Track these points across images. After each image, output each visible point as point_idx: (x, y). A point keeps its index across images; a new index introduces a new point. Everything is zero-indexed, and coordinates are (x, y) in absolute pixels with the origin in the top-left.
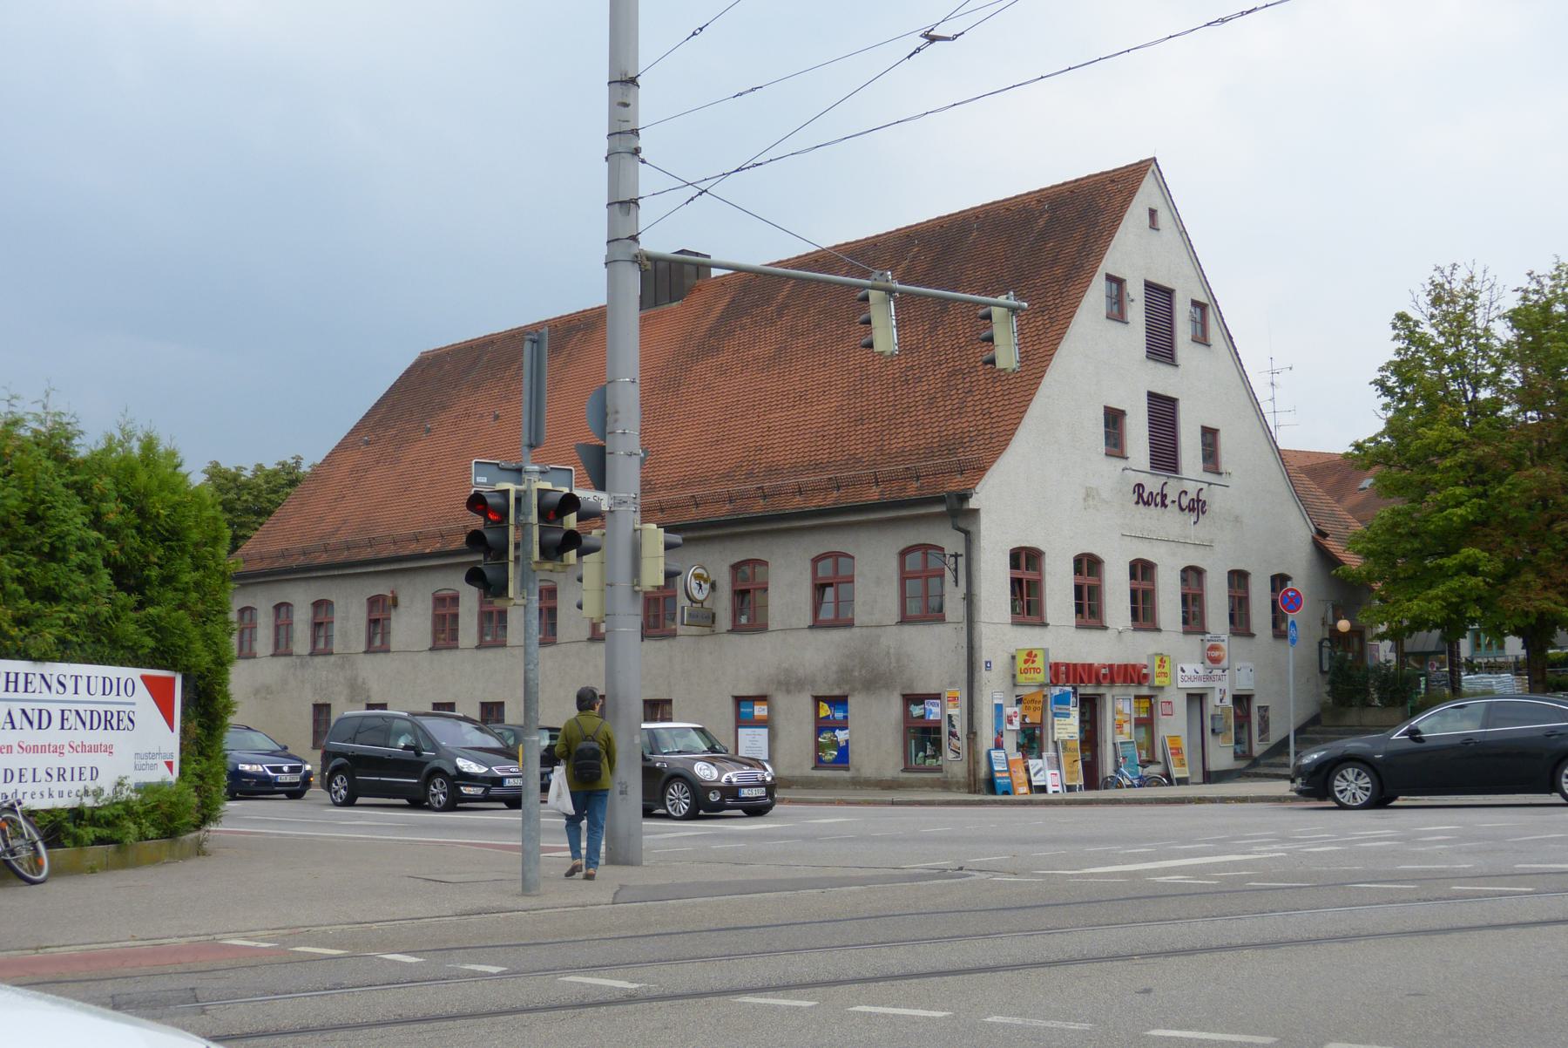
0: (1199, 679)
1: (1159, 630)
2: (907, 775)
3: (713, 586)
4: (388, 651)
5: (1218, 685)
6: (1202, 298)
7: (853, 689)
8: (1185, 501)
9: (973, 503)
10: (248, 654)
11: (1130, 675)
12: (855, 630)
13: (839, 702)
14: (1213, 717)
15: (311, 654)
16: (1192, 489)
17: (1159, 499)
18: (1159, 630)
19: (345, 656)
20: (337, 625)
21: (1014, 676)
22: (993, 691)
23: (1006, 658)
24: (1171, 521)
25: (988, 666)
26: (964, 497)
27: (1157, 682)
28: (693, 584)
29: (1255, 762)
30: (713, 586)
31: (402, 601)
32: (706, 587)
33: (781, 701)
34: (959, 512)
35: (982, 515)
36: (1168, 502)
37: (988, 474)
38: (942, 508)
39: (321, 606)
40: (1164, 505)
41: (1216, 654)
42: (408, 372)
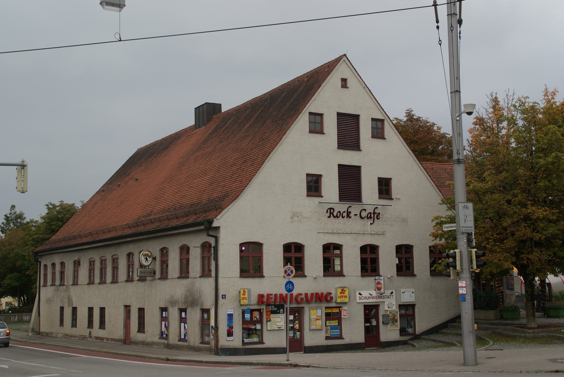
0: (373, 298)
1: (344, 276)
2: (201, 345)
3: (154, 259)
4: (77, 284)
5: (387, 301)
6: (380, 116)
7: (188, 306)
8: (364, 214)
9: (215, 225)
10: (45, 285)
11: (321, 298)
12: (189, 279)
13: (185, 310)
14: (383, 316)
15: (127, 281)
16: (370, 209)
17: (345, 214)
18: (344, 276)
19: (67, 286)
20: (66, 273)
21: (240, 301)
22: (227, 308)
23: (236, 293)
24: (355, 224)
25: (224, 297)
26: (211, 222)
27: (339, 300)
28: (143, 259)
29: (416, 337)
30: (154, 259)
31: (82, 263)
32: (150, 259)
33: (170, 310)
34: (210, 229)
35: (221, 229)
36: (352, 215)
37: (224, 211)
38: (202, 227)
39: (62, 264)
40: (348, 216)
41: (379, 286)
42: (130, 158)
